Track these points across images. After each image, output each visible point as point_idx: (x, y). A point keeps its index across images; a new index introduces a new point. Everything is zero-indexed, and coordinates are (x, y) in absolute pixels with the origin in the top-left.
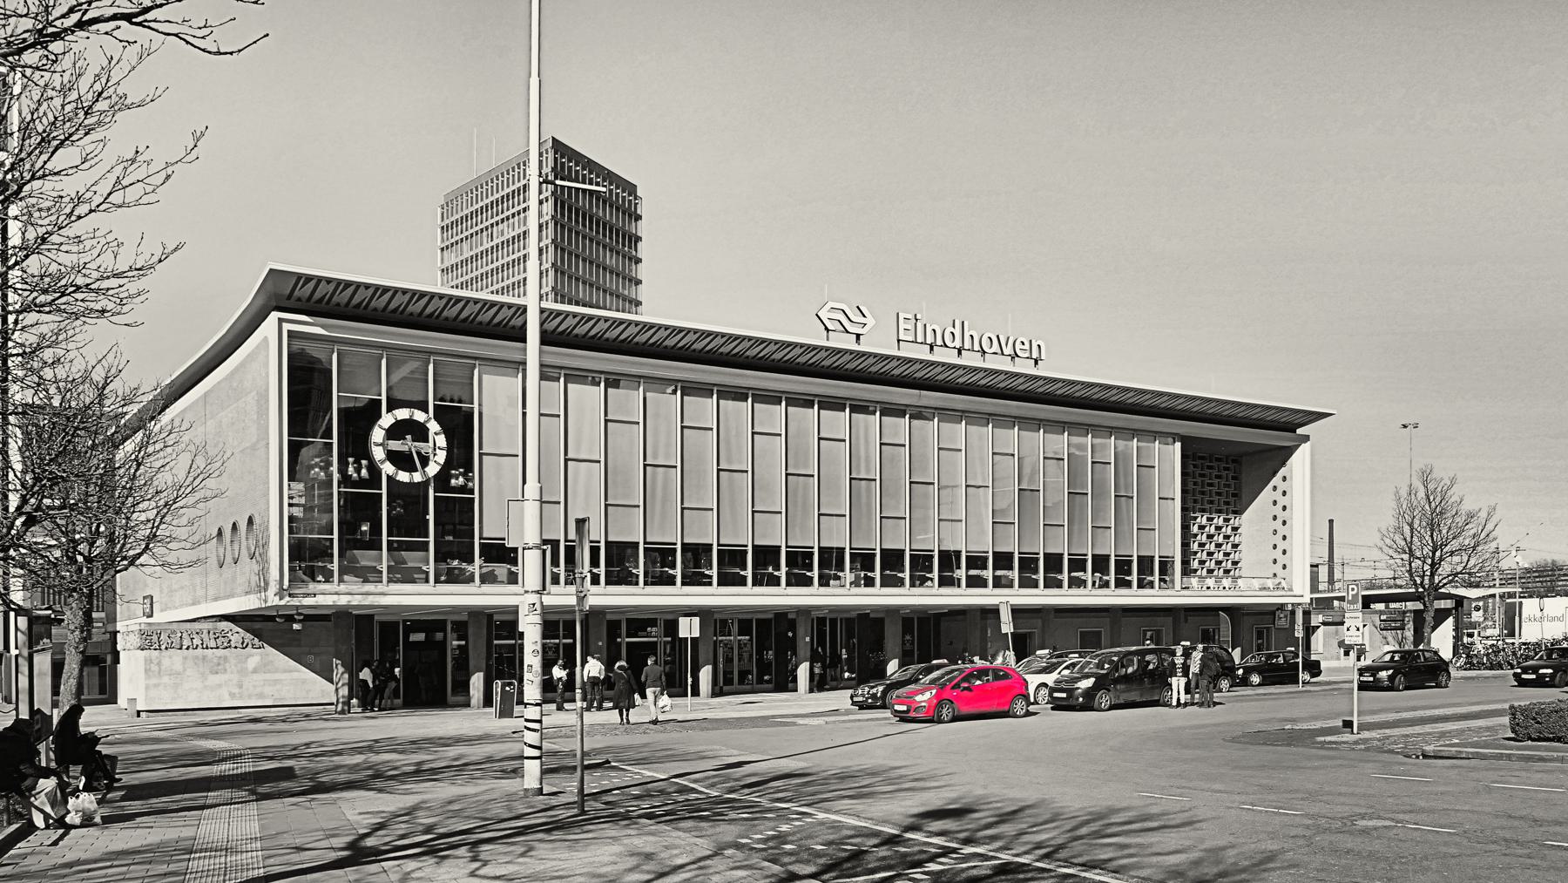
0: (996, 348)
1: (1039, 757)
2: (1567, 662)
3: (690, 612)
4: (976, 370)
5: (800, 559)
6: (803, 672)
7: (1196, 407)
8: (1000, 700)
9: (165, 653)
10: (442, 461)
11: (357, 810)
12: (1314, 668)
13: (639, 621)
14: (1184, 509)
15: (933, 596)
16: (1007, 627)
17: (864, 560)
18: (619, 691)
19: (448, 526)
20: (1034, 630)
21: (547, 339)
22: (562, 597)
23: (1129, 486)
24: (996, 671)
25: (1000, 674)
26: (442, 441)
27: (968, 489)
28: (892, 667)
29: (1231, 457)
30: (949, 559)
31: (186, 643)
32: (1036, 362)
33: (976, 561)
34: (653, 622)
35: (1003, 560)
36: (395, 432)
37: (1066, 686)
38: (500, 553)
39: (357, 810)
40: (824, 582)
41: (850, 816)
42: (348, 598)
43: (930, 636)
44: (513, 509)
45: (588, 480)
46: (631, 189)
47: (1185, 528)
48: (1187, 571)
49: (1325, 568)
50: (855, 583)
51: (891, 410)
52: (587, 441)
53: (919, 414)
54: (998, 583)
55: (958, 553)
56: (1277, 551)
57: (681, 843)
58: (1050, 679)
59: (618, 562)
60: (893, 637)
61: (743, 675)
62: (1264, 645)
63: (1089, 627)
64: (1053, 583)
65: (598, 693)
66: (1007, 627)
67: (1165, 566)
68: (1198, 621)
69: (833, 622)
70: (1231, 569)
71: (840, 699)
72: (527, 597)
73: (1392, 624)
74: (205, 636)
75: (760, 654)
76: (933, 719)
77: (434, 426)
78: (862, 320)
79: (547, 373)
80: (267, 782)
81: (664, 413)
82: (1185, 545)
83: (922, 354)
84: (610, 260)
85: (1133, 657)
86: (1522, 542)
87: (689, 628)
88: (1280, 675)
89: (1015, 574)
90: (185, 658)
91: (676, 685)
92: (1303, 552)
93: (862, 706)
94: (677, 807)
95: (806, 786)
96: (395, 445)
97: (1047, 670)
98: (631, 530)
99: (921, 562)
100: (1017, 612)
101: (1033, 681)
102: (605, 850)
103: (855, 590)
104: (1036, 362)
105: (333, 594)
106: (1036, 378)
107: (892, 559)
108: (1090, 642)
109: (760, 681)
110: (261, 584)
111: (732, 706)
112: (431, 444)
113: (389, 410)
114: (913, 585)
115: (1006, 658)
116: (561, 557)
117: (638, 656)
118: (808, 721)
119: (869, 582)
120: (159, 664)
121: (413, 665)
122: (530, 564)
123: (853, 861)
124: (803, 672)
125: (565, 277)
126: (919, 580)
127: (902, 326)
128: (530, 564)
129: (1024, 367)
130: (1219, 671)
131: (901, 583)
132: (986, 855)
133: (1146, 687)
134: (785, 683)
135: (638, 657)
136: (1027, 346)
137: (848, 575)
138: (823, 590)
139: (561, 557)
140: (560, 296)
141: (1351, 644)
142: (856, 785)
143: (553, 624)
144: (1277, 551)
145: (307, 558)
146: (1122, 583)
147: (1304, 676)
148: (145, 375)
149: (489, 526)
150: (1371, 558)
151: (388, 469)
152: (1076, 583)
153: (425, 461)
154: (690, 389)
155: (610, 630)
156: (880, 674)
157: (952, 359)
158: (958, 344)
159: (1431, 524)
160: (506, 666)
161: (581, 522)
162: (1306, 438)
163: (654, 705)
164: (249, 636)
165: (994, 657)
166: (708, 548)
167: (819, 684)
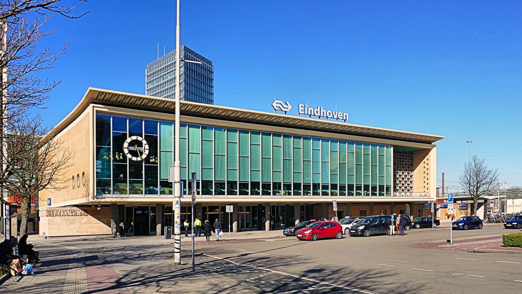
0: (331, 116)
1: (347, 252)
3: (230, 204)
4: (325, 123)
5: (266, 186)
6: (267, 224)
8: (331, 233)
9: (55, 217)
10: (147, 154)
11: (119, 270)
12: (437, 222)
13: (213, 207)
16: (335, 209)
18: (206, 230)
19: (150, 176)
20: (344, 210)
22: (188, 199)
24: (332, 223)
25: (334, 224)
26: (147, 147)
28: (297, 222)
29: (409, 154)
30: (316, 186)
31: (62, 214)
32: (345, 121)
33: (325, 187)
34: (217, 207)
35: (334, 187)
36: (132, 144)
37: (355, 228)
38: (167, 184)
39: (119, 270)
40: (274, 194)
41: (282, 272)
42: (116, 199)
43: (309, 211)
45: (196, 160)
46: (210, 63)
47: (395, 176)
48: (395, 190)
50: (285, 194)
51: (297, 137)
53: (306, 138)
54: (332, 194)
56: (426, 183)
57: (227, 281)
58: (350, 226)
61: (247, 225)
62: (421, 215)
63: (362, 209)
65: (199, 231)
66: (335, 209)
67: (388, 189)
68: (399, 207)
69: (277, 207)
70: (410, 189)
71: (280, 233)
72: (175, 199)
74: (68, 212)
75: (253, 218)
76: (310, 239)
77: (144, 142)
78: (286, 106)
79: (182, 125)
81: (222, 139)
82: (395, 181)
85: (377, 220)
86: (506, 181)
87: (229, 209)
88: (426, 224)
89: (338, 191)
90: (62, 219)
91: (225, 228)
92: (434, 183)
93: (287, 235)
94: (225, 269)
95: (268, 262)
96: (132, 148)
99: (307, 187)
100: (339, 204)
101: (344, 227)
102: (201, 283)
103: (285, 196)
104: (345, 121)
107: (297, 186)
108: (363, 214)
109: (253, 227)
110: (87, 194)
111: (244, 235)
112: (143, 148)
113: (129, 137)
116: (187, 185)
117: (212, 218)
118: (269, 240)
119: (289, 194)
120: (53, 221)
122: (177, 188)
123: (284, 287)
124: (267, 224)
125: (188, 94)
126: (306, 193)
127: (300, 108)
128: (177, 188)
130: (406, 223)
131: (300, 194)
133: (380, 228)
134: (261, 227)
135: (213, 219)
136: (342, 115)
137: (282, 192)
138: (274, 196)
140: (186, 99)
143: (184, 208)
144: (426, 183)
146: (374, 194)
147: (434, 225)
148: (49, 124)
149: (162, 176)
150: (457, 186)
151: (129, 156)
152: (358, 194)
153: (141, 153)
155: (203, 210)
156: (293, 224)
158: (309, 114)
159: (477, 177)
160: (169, 222)
161: (193, 174)
162: (435, 146)
163: (218, 235)
164: (83, 212)
165: (331, 219)
167: (273, 228)
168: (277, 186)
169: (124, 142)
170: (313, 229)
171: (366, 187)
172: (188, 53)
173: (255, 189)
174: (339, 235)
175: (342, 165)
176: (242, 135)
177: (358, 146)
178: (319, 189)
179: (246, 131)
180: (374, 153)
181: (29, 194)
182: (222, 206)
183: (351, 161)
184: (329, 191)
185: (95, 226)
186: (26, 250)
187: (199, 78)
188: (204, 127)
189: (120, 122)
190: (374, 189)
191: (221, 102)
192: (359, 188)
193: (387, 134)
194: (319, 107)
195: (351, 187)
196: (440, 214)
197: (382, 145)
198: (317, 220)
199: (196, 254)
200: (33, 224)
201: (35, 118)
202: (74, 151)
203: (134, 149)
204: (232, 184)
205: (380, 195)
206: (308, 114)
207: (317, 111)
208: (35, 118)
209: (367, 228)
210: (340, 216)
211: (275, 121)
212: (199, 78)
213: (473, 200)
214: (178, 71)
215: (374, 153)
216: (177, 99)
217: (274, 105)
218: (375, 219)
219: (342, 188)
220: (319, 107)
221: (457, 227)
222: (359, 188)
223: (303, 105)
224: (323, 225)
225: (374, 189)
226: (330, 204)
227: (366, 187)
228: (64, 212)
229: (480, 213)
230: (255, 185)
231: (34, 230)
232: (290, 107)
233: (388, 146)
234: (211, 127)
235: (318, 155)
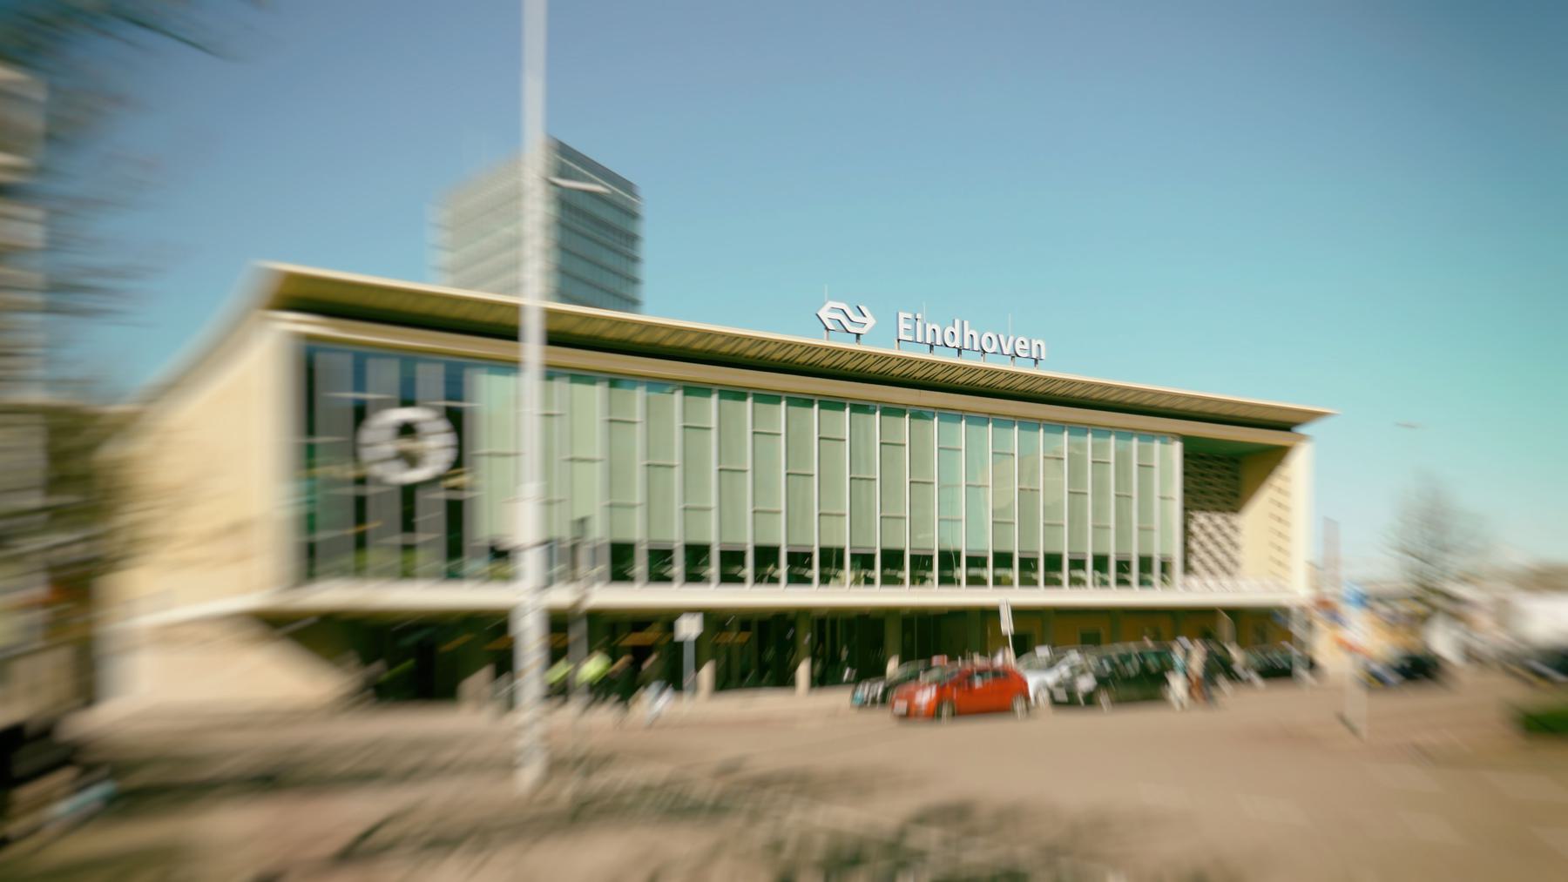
0: (995, 347)
1: (1044, 757)
2: (1567, 662)
3: (693, 611)
4: (976, 370)
5: (799, 560)
6: (803, 671)
7: (1196, 407)
8: (1002, 697)
11: (355, 811)
12: (1312, 665)
13: (640, 620)
14: (1186, 509)
15: (933, 596)
16: (1007, 626)
17: (864, 561)
18: (619, 687)
19: (450, 528)
20: (1035, 628)
21: (556, 338)
22: (562, 596)
23: (1128, 485)
24: (996, 673)
25: (1002, 675)
27: (970, 492)
28: (893, 667)
29: (1229, 462)
30: (949, 559)
32: (959, 351)
33: (976, 561)
35: (1003, 560)
37: (1069, 687)
38: (500, 554)
39: (355, 811)
40: (825, 580)
41: (846, 817)
43: (930, 635)
44: (517, 513)
45: (591, 481)
46: (627, 186)
47: (1186, 527)
48: (1187, 569)
49: (1322, 569)
50: (856, 581)
51: (892, 410)
52: (593, 441)
53: (919, 414)
54: (998, 581)
55: (841, 552)
56: (1275, 552)
57: (683, 843)
58: (1050, 678)
59: (620, 561)
60: (893, 636)
61: (744, 675)
62: (1259, 643)
63: (1085, 627)
64: (1052, 582)
65: (602, 689)
66: (1007, 626)
67: (1165, 567)
68: (1199, 621)
69: (834, 622)
70: (1229, 567)
71: (838, 699)
72: (527, 597)
73: (1392, 623)
75: (758, 652)
76: (934, 714)
78: (860, 319)
79: (551, 373)
80: (270, 779)
81: (666, 417)
82: (1186, 544)
83: (923, 355)
84: (609, 259)
85: (1133, 655)
86: (1523, 541)
87: (688, 629)
88: (1277, 672)
89: (1015, 573)
91: (674, 679)
92: (1303, 547)
93: (863, 704)
94: (675, 806)
95: (805, 785)
97: (1051, 665)
98: (636, 532)
99: (921, 562)
100: (1019, 613)
101: (1033, 681)
102: (605, 849)
103: (855, 589)
104: (959, 351)
105: (335, 594)
106: (1036, 378)
107: (892, 559)
108: (1089, 640)
109: (761, 675)
110: (259, 582)
111: (738, 705)
114: (913, 582)
115: (1005, 658)
116: (563, 557)
117: (640, 653)
118: (805, 716)
119: (869, 581)
121: (422, 662)
122: (530, 564)
123: (854, 860)
124: (803, 671)
125: (568, 281)
126: (919, 580)
127: (902, 325)
128: (530, 564)
129: (1024, 368)
130: (1219, 667)
131: (900, 582)
132: (979, 855)
133: (1142, 684)
134: (784, 679)
135: (637, 654)
136: (1026, 346)
137: (847, 573)
138: (824, 589)
139: (563, 557)
140: (564, 297)
141: (1349, 644)
142: (853, 784)
143: (558, 623)
144: (1275, 552)
145: (312, 560)
146: (1122, 582)
147: (1301, 671)
148: (155, 373)
149: (484, 527)
150: (1375, 561)
152: (1076, 582)
154: (694, 389)
155: (608, 629)
156: (878, 671)
157: (952, 359)
158: (929, 341)
159: (1432, 528)
160: (504, 663)
161: (583, 521)
162: (1303, 438)
163: (654, 703)
165: (994, 655)
166: (901, 554)
167: (821, 681)
168: (832, 559)
169: (374, 355)
170: (941, 690)
171: (1101, 563)
172: (567, 159)
173: (766, 565)
174: (1019, 706)
175: (1027, 494)
176: (730, 404)
177: (1078, 439)
178: (959, 565)
179: (738, 394)
180: (1123, 459)
181: (76, 588)
182: (668, 619)
183: (1053, 486)
184: (988, 573)
185: (288, 683)
186: (78, 760)
187: (596, 229)
188: (614, 381)
189: (361, 357)
190: (1123, 566)
191: (664, 305)
192: (1078, 564)
193: (1147, 401)
194: (957, 322)
195: (1053, 562)
196: (1324, 648)
197: (1148, 435)
198: (952, 658)
199: (589, 763)
200: (87, 685)
201: (106, 356)
202: (219, 461)
203: (400, 447)
204: (697, 554)
205: (1143, 583)
206: (924, 343)
207: (932, 329)
208: (106, 356)
209: (1102, 682)
210: (1022, 645)
211: (874, 369)
212: (596, 229)
213: (1428, 601)
214: (536, 212)
215: (1123, 459)
216: (533, 297)
217: (825, 314)
218: (1125, 658)
219: (1028, 564)
220: (957, 322)
221: (1375, 680)
222: (1078, 564)
223: (910, 316)
224: (969, 677)
225: (1123, 566)
226: (991, 614)
227: (1101, 563)
228: (194, 630)
229: (1442, 641)
230: (766, 555)
231: (321, 359)
232: (870, 321)
233: (1165, 436)
234: (635, 380)
235: (1084, 505)
